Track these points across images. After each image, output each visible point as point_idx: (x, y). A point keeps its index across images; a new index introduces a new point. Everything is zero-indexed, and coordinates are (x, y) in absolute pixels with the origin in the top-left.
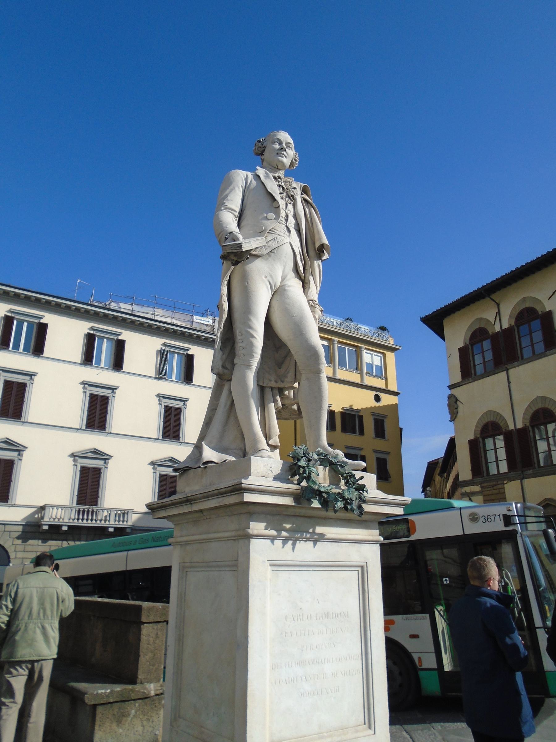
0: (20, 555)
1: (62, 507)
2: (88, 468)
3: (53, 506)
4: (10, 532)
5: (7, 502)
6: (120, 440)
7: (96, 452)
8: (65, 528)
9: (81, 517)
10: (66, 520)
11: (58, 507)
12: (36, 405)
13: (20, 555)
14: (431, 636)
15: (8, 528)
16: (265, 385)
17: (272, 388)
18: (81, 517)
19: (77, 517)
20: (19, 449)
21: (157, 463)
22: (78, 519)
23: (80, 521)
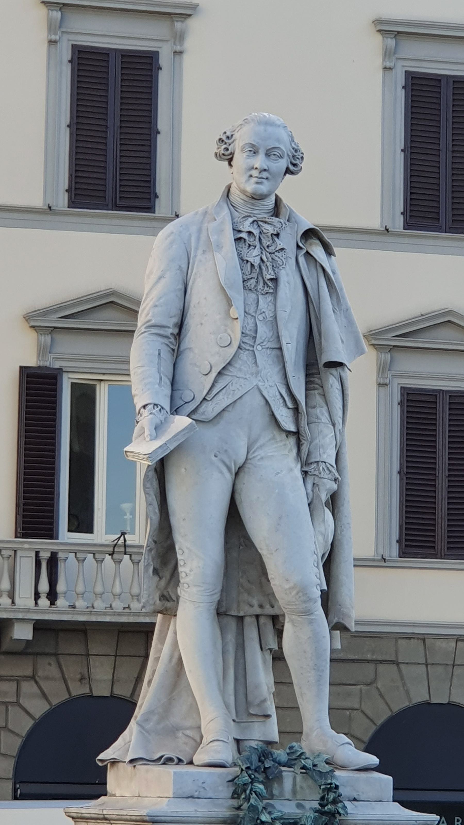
16: (241, 614)
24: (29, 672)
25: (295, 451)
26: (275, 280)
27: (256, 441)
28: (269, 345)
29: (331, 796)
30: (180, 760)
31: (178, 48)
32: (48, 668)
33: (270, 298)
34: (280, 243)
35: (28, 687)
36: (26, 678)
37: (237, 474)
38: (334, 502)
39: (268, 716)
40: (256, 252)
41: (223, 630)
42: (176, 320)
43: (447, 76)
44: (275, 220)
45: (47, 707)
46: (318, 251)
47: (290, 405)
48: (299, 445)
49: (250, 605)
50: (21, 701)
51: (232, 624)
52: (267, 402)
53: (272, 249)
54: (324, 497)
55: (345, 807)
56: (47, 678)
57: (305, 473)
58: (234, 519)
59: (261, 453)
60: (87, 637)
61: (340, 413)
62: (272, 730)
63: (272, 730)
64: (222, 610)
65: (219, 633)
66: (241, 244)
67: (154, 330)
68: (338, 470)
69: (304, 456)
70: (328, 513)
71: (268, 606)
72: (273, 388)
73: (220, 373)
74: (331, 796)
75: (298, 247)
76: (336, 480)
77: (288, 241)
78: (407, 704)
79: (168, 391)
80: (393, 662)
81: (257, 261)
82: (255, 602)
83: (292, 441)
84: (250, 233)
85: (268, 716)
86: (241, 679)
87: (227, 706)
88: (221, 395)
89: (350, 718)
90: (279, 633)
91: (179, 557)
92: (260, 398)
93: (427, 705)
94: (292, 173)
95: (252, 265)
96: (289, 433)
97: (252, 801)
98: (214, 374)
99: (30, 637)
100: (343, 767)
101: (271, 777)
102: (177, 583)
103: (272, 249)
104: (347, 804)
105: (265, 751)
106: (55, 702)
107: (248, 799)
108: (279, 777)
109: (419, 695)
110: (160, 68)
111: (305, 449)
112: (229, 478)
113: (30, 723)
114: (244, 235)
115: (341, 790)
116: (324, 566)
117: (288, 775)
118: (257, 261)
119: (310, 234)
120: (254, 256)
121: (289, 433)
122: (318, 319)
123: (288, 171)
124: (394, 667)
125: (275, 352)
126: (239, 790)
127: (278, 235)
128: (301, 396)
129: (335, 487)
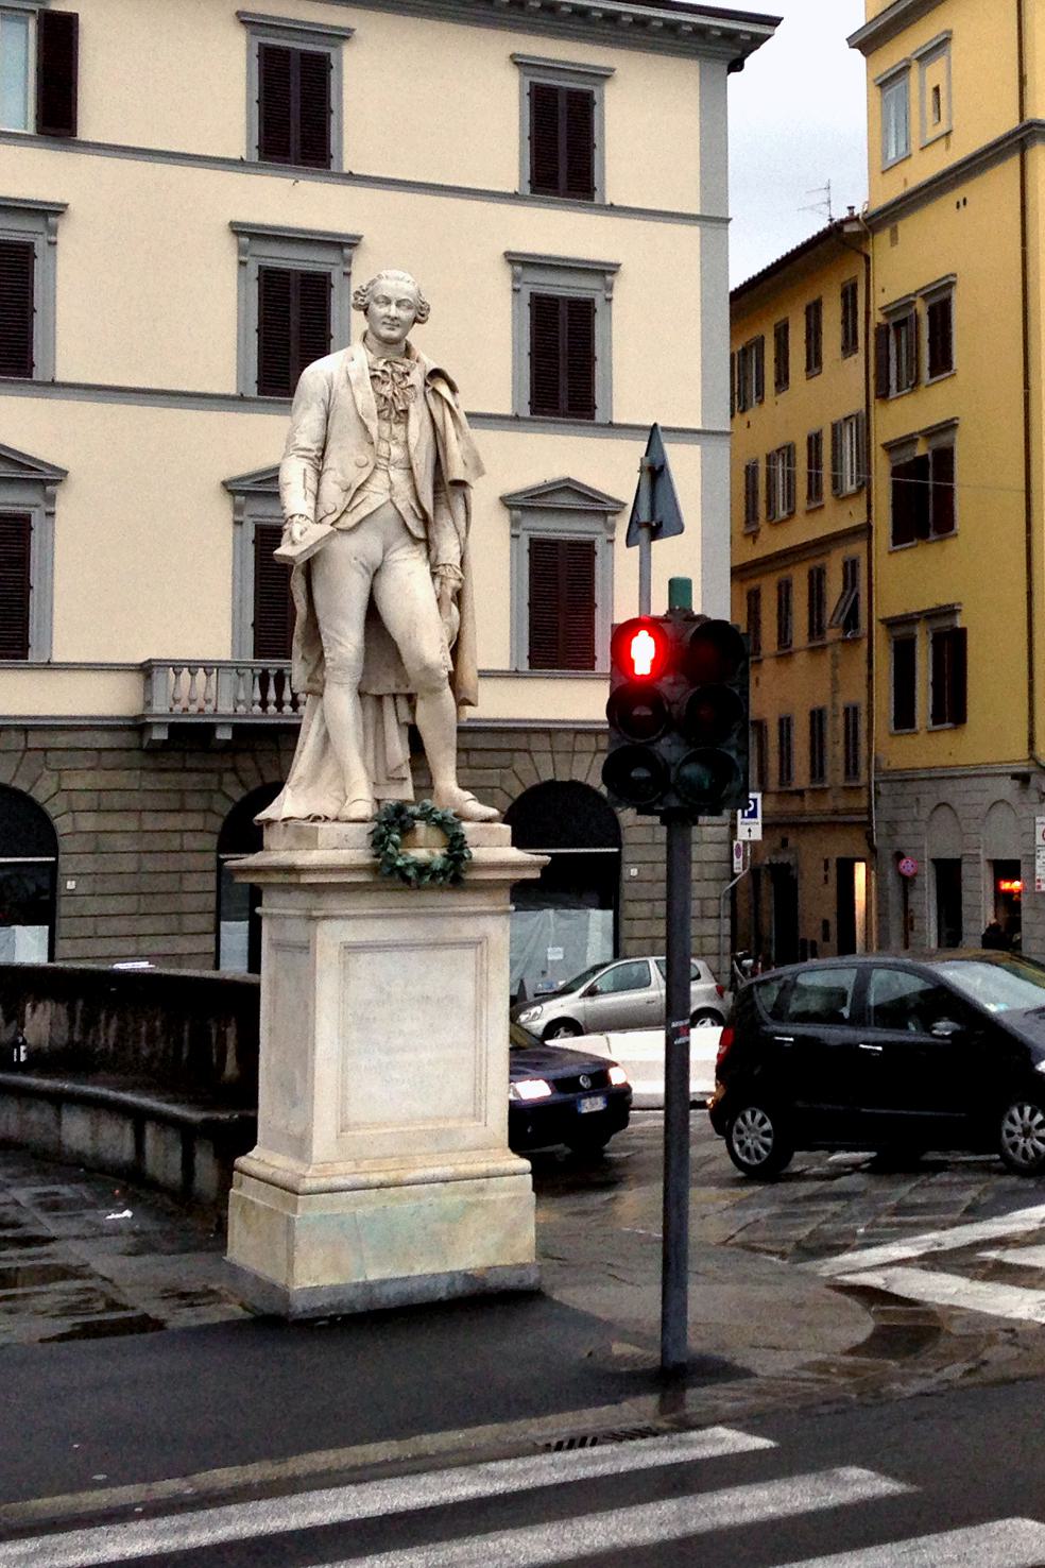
0: (88, 822)
1: (208, 666)
2: (554, 544)
3: (177, 666)
4: (45, 750)
5: (592, 667)
6: (115, 408)
7: (568, 487)
8: (225, 734)
9: (272, 695)
10: (226, 708)
11: (193, 666)
12: (78, 318)
13: (88, 822)
14: (260, 1098)
15: (35, 740)
17: (395, 696)
18: (272, 695)
19: (258, 696)
20: (43, 478)
21: (247, 486)
22: (264, 704)
23: (272, 709)
24: (229, 765)
25: (425, 555)
26: (406, 412)
27: (391, 546)
28: (402, 466)
29: (458, 843)
30: (327, 818)
31: (347, 270)
32: (245, 762)
33: (402, 426)
34: (410, 380)
35: (228, 777)
36: (226, 770)
37: (374, 575)
38: (459, 597)
39: (405, 779)
40: (388, 387)
41: (363, 705)
42: (320, 445)
43: (562, 297)
44: (406, 360)
45: (244, 793)
46: (444, 389)
47: (420, 516)
48: (428, 550)
49: (387, 684)
50: (223, 787)
51: (370, 701)
52: (399, 513)
53: (403, 385)
54: (449, 593)
55: (470, 852)
56: (245, 771)
57: (434, 575)
58: (373, 616)
59: (395, 556)
60: (320, 767)
61: (464, 524)
62: (407, 792)
63: (407, 792)
64: (363, 689)
65: (360, 707)
66: (376, 381)
67: (302, 453)
68: (462, 571)
69: (433, 560)
70: (454, 608)
71: (403, 686)
72: (404, 502)
73: (358, 489)
74: (458, 843)
75: (426, 384)
76: (460, 580)
77: (416, 378)
78: (536, 782)
79: (312, 504)
80: (525, 751)
81: (390, 395)
82: (393, 684)
83: (422, 546)
84: (383, 371)
85: (405, 779)
86: (380, 749)
87: (366, 768)
88: (359, 508)
89: (493, 794)
90: (413, 709)
91: (324, 645)
92: (393, 511)
93: (552, 784)
94: (420, 322)
95: (386, 399)
96: (420, 540)
97: (389, 850)
98: (353, 491)
99: (230, 737)
100: (468, 820)
101: (407, 830)
102: (324, 668)
103: (403, 385)
104: (471, 849)
105: (400, 809)
106: (252, 788)
107: (385, 849)
108: (412, 829)
109: (547, 776)
110: (332, 286)
111: (433, 553)
112: (368, 578)
113: (230, 807)
114: (379, 373)
115: (466, 839)
116: (451, 652)
117: (420, 825)
118: (390, 395)
119: (437, 374)
120: (387, 390)
121: (415, 540)
122: (444, 445)
123: (416, 320)
124: (527, 755)
125: (406, 472)
126: (378, 841)
127: (408, 374)
128: (428, 505)
129: (459, 585)
